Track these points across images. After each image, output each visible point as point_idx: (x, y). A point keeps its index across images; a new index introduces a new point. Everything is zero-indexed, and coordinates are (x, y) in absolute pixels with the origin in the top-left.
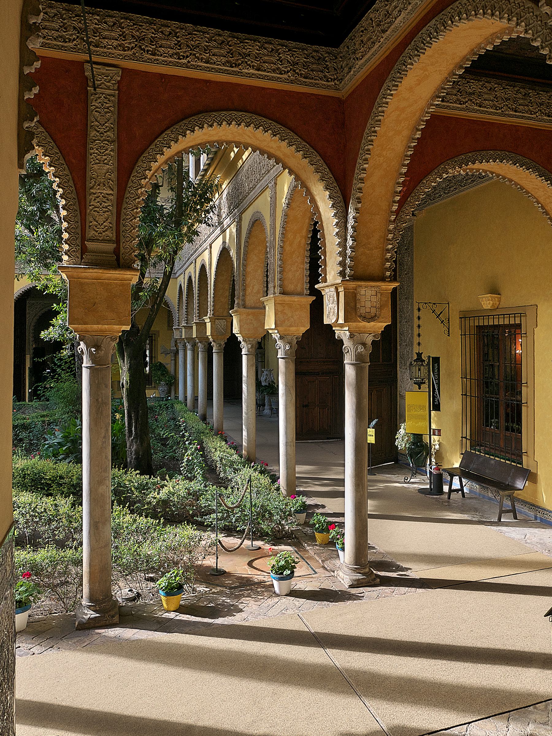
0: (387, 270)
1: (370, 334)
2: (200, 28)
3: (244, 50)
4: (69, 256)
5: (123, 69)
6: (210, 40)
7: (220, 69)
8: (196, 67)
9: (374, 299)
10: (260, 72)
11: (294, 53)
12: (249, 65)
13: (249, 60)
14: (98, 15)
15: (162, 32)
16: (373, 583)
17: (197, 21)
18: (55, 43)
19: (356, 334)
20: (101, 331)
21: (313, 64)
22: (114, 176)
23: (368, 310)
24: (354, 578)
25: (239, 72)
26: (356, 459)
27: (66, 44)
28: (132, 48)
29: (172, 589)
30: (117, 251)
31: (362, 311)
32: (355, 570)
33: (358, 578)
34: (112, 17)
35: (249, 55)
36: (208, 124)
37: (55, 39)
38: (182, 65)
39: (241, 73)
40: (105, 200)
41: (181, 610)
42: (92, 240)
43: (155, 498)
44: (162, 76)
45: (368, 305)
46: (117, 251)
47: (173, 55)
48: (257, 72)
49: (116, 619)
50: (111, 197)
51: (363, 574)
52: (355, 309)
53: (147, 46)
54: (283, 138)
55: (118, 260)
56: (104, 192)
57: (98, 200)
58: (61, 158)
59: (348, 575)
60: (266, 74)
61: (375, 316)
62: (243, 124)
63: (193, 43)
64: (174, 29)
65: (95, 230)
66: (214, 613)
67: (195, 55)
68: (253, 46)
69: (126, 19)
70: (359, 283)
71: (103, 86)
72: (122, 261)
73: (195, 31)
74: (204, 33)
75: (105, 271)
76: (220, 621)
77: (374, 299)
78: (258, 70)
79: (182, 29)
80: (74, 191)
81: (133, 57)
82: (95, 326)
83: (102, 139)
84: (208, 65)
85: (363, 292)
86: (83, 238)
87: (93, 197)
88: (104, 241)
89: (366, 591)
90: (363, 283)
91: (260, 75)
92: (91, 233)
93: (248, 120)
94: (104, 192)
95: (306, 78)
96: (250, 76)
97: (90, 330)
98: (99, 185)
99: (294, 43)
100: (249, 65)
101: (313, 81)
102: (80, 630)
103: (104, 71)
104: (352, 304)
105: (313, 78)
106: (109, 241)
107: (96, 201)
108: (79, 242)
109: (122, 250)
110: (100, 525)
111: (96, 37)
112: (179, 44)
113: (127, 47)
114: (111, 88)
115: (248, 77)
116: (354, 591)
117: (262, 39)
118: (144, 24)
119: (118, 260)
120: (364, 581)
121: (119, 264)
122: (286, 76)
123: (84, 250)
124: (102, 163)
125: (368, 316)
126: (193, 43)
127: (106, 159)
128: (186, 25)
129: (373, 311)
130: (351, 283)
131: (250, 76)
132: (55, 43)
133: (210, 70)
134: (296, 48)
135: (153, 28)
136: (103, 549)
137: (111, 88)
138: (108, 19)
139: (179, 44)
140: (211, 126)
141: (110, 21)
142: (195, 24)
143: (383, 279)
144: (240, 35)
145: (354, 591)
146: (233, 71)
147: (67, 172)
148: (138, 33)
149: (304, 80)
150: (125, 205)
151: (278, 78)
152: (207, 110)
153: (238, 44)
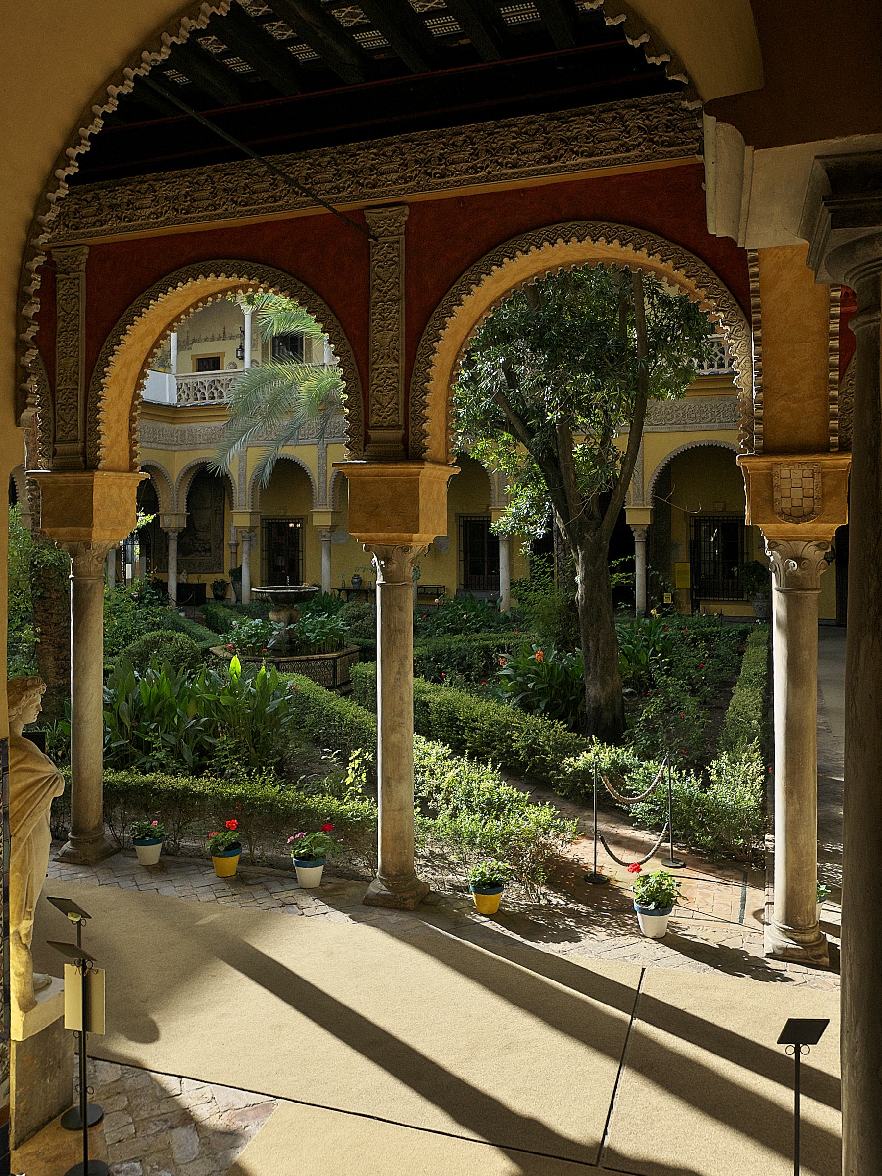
0: (833, 432)
1: (809, 542)
2: (504, 121)
3: (569, 134)
4: (351, 450)
5: (410, 205)
6: (519, 134)
7: (533, 170)
8: (498, 178)
9: (809, 484)
10: (593, 159)
11: (650, 113)
12: (576, 153)
13: (575, 145)
14: (375, 148)
15: (453, 144)
16: (815, 961)
17: (498, 114)
18: (328, 196)
19: (782, 542)
20: (389, 539)
21: (682, 120)
22: (402, 342)
23: (796, 503)
24: (780, 944)
25: (561, 167)
26: (786, 749)
27: (340, 195)
28: (416, 176)
29: (484, 885)
30: (405, 440)
31: (785, 504)
32: (785, 932)
33: (785, 945)
34: (390, 144)
35: (576, 138)
36: (521, 251)
37: (394, 183)
38: (480, 180)
39: (566, 166)
40: (389, 375)
41: (498, 916)
42: (374, 428)
43: (571, 766)
44: (460, 199)
45: (798, 493)
46: (405, 440)
47: (618, 148)
48: (588, 159)
49: (410, 903)
50: (396, 371)
51: (798, 942)
52: (771, 501)
53: (433, 168)
54: (639, 246)
55: (406, 450)
56: (389, 365)
57: (381, 376)
58: (342, 332)
59: (771, 937)
60: (604, 157)
61: (812, 512)
62: (574, 239)
63: (494, 145)
64: (469, 134)
65: (378, 415)
66: (534, 932)
67: (497, 161)
68: (581, 125)
69: (407, 141)
70: (774, 459)
71: (386, 232)
72: (411, 451)
73: (499, 127)
74: (510, 126)
75: (385, 466)
76: (541, 946)
77: (809, 484)
78: (590, 155)
79: (479, 131)
80: (356, 369)
81: (419, 188)
82: (381, 534)
83: (385, 300)
84: (516, 170)
85: (785, 473)
86: (367, 426)
87: (376, 374)
88: (389, 427)
89: (790, 969)
90: (781, 459)
91: (595, 162)
92: (374, 419)
93: (581, 232)
94: (389, 365)
95: (671, 145)
96: (579, 167)
97: (376, 538)
98: (382, 358)
99: (651, 97)
100: (576, 153)
101: (684, 147)
102: (366, 905)
103: (387, 214)
104: (766, 494)
105: (683, 142)
106: (396, 427)
107: (380, 378)
108: (361, 430)
109: (411, 437)
110: (393, 783)
111: (589, 143)
112: (548, 143)
113: (632, 145)
114: (396, 233)
115: (577, 170)
116: (774, 964)
117: (597, 107)
118: (501, 130)
119: (406, 450)
120: (795, 953)
121: (407, 454)
122: (636, 152)
123: (367, 440)
124: (387, 329)
125: (796, 513)
126: (494, 145)
127: (390, 324)
128: (486, 123)
129: (808, 504)
130: (758, 460)
131: (579, 167)
132: (328, 196)
133: (519, 175)
134: (654, 104)
135: (442, 142)
136: (396, 813)
137: (396, 233)
138: (604, 115)
139: (475, 154)
140: (526, 252)
141: (388, 150)
142: (497, 118)
143: (825, 449)
144: (564, 113)
145: (774, 964)
146: (553, 168)
147: (348, 347)
148: (422, 156)
149: (668, 149)
150: (413, 379)
151: (624, 158)
152: (521, 231)
153: (560, 126)
